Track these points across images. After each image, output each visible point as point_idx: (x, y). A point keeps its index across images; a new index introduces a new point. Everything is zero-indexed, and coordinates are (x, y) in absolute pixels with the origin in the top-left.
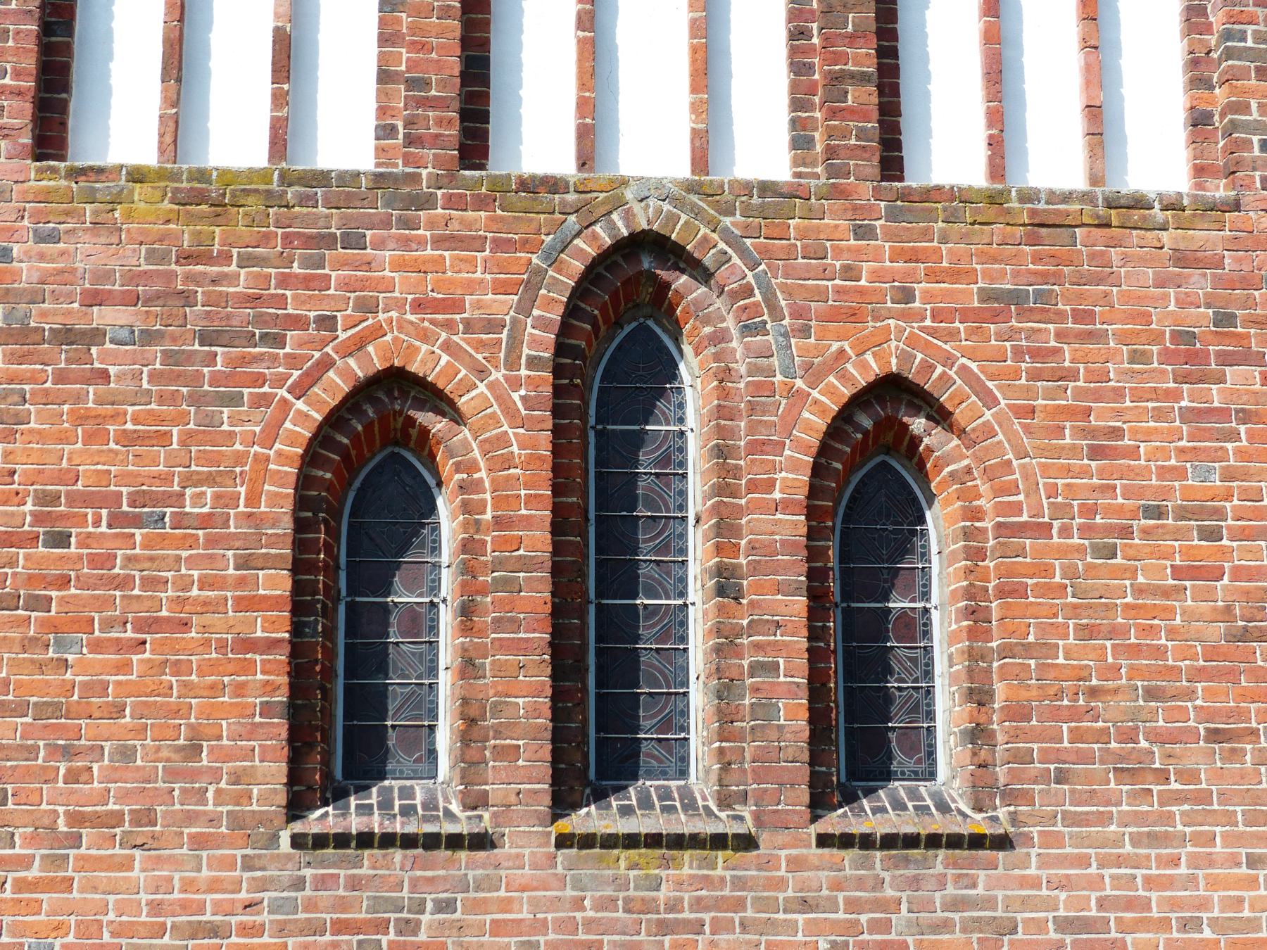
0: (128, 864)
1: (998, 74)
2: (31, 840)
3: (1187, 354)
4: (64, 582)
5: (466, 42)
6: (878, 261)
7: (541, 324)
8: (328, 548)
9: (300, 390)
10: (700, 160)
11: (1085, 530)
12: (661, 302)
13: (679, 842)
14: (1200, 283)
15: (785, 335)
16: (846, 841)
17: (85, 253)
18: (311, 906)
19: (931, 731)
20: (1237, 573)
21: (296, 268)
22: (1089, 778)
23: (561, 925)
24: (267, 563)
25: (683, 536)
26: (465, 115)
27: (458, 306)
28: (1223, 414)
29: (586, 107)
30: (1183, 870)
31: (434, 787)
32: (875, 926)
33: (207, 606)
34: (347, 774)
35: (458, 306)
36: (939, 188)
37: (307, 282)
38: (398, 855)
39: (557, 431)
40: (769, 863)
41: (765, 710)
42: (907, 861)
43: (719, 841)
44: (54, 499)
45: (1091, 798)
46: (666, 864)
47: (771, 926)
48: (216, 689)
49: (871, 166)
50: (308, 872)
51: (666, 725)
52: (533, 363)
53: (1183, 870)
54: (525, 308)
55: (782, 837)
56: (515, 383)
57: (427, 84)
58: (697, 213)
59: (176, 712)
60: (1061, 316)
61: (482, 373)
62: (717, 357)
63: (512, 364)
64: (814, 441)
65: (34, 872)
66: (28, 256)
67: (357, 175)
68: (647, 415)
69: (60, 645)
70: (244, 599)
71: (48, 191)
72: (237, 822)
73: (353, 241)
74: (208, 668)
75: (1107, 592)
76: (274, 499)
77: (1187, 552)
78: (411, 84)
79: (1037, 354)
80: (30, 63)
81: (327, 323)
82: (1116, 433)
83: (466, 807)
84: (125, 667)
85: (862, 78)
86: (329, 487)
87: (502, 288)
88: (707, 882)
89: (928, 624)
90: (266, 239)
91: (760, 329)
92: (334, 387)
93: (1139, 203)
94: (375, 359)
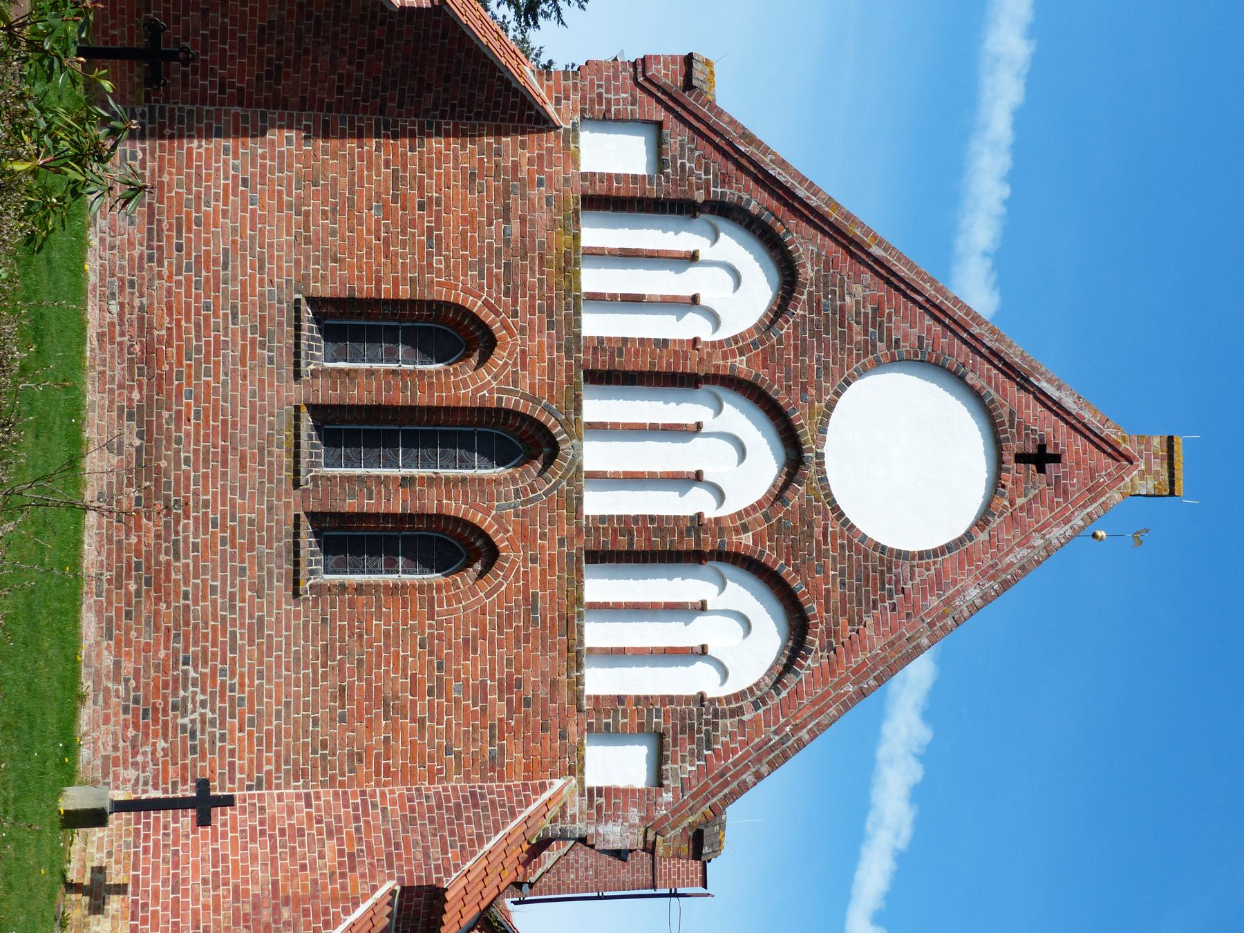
0: (288, 234)
1: (633, 301)
2: (298, 196)
3: (510, 685)
4: (404, 209)
5: (641, 373)
6: (549, 548)
7: (517, 402)
8: (420, 316)
9: (486, 303)
10: (592, 475)
11: (431, 636)
12: (529, 458)
13: (297, 456)
14: (543, 692)
15: (515, 507)
16: (297, 526)
17: (542, 216)
18: (271, 306)
19: (346, 573)
20: (414, 703)
21: (538, 302)
22: (324, 632)
23: (262, 407)
24: (413, 290)
25: (429, 467)
26: (609, 372)
27: (524, 368)
28: (484, 699)
29: (615, 426)
30: (284, 672)
31: (319, 358)
32: (261, 538)
33: (395, 265)
34: (326, 325)
35: (524, 368)
36: (582, 576)
37: (532, 306)
38: (292, 341)
39: (472, 410)
40: (288, 495)
41: (352, 495)
42: (288, 552)
43: (297, 473)
44: (438, 205)
45: (315, 633)
46: (288, 451)
47: (261, 494)
48: (360, 269)
49: (592, 546)
50: (285, 305)
51: (348, 458)
52: (500, 399)
53: (284, 672)
54: (523, 396)
55: (299, 500)
56: (491, 392)
57: (620, 356)
58: (568, 470)
59: (350, 253)
60: (526, 628)
61: (495, 378)
62: (505, 479)
63: (499, 390)
64: (469, 518)
65: (285, 198)
66: (540, 193)
67: (580, 327)
68: (481, 454)
69: (378, 208)
70: (399, 277)
71: (568, 202)
72: (306, 277)
73: (551, 325)
74: (369, 265)
75: (405, 644)
76: (440, 292)
77: (422, 680)
78: (620, 350)
79: (509, 617)
80: (623, 193)
81: (515, 314)
82: (475, 651)
83: (312, 371)
84: (369, 233)
85: (631, 543)
86: (446, 316)
87: (532, 386)
88: (280, 468)
89: (392, 573)
90: (550, 289)
91: (517, 496)
92: (489, 318)
93: (579, 666)
94: (501, 334)
